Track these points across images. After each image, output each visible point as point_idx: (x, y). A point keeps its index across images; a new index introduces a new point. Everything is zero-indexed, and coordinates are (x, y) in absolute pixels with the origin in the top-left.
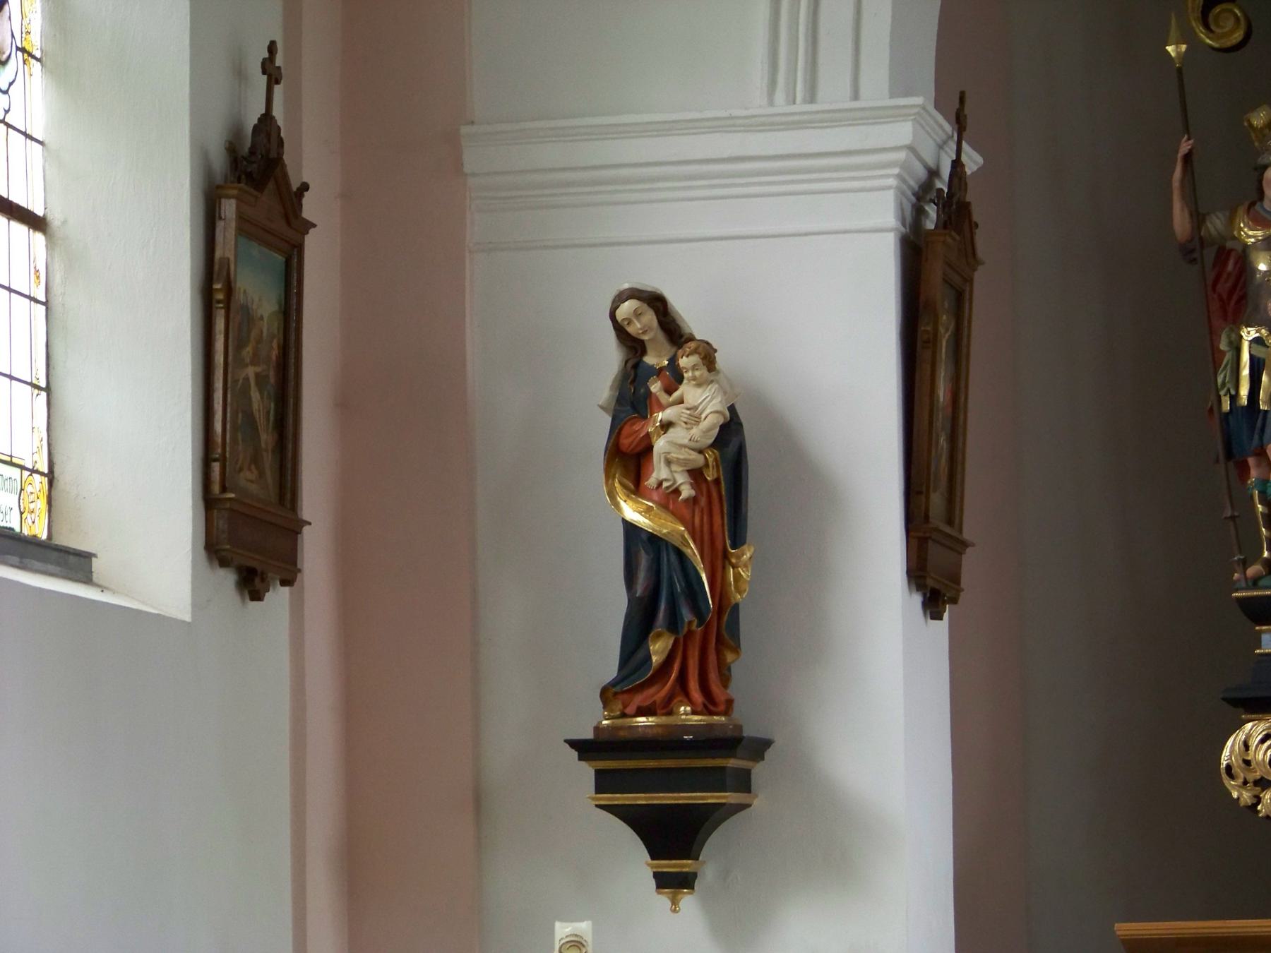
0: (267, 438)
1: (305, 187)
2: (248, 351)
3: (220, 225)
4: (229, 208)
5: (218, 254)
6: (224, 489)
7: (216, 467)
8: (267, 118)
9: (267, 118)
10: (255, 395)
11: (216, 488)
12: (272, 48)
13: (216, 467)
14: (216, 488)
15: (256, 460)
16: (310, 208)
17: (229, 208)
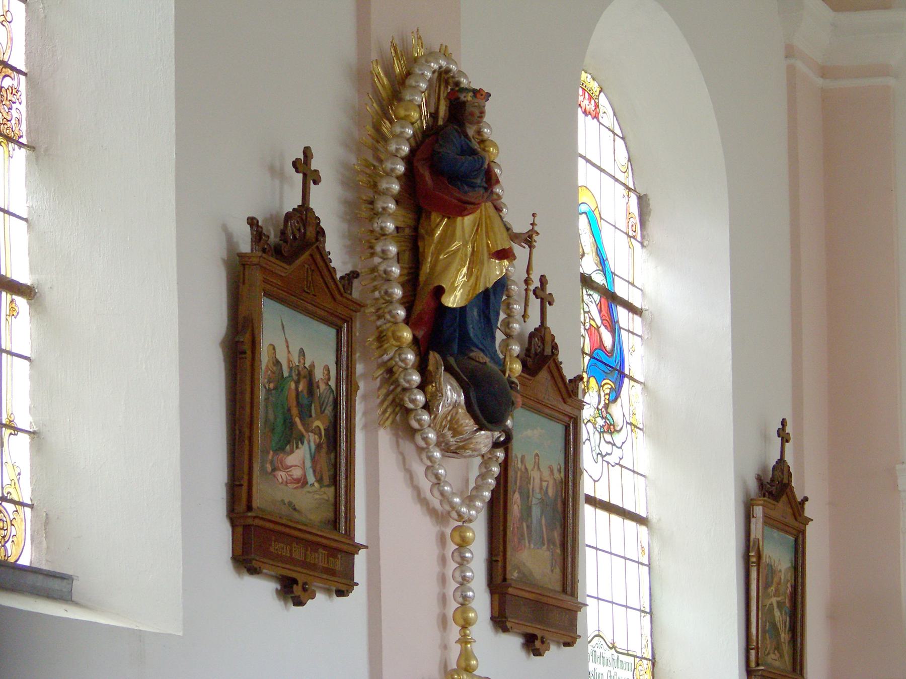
0: (785, 636)
1: (806, 499)
2: (772, 588)
3: (753, 520)
4: (758, 511)
5: (752, 537)
6: (758, 665)
7: (753, 653)
8: (781, 461)
9: (781, 461)
10: (777, 613)
11: (753, 664)
12: (784, 423)
13: (753, 653)
14: (753, 664)
15: (778, 648)
16: (809, 510)
17: (758, 511)
